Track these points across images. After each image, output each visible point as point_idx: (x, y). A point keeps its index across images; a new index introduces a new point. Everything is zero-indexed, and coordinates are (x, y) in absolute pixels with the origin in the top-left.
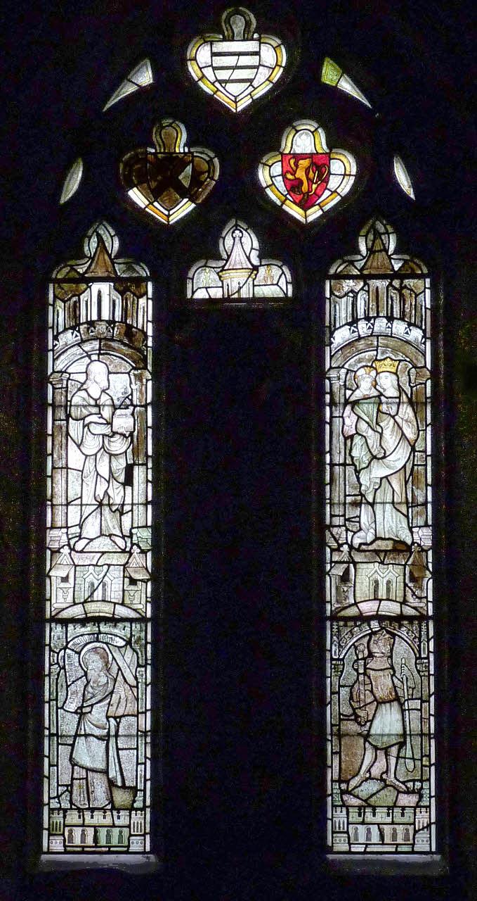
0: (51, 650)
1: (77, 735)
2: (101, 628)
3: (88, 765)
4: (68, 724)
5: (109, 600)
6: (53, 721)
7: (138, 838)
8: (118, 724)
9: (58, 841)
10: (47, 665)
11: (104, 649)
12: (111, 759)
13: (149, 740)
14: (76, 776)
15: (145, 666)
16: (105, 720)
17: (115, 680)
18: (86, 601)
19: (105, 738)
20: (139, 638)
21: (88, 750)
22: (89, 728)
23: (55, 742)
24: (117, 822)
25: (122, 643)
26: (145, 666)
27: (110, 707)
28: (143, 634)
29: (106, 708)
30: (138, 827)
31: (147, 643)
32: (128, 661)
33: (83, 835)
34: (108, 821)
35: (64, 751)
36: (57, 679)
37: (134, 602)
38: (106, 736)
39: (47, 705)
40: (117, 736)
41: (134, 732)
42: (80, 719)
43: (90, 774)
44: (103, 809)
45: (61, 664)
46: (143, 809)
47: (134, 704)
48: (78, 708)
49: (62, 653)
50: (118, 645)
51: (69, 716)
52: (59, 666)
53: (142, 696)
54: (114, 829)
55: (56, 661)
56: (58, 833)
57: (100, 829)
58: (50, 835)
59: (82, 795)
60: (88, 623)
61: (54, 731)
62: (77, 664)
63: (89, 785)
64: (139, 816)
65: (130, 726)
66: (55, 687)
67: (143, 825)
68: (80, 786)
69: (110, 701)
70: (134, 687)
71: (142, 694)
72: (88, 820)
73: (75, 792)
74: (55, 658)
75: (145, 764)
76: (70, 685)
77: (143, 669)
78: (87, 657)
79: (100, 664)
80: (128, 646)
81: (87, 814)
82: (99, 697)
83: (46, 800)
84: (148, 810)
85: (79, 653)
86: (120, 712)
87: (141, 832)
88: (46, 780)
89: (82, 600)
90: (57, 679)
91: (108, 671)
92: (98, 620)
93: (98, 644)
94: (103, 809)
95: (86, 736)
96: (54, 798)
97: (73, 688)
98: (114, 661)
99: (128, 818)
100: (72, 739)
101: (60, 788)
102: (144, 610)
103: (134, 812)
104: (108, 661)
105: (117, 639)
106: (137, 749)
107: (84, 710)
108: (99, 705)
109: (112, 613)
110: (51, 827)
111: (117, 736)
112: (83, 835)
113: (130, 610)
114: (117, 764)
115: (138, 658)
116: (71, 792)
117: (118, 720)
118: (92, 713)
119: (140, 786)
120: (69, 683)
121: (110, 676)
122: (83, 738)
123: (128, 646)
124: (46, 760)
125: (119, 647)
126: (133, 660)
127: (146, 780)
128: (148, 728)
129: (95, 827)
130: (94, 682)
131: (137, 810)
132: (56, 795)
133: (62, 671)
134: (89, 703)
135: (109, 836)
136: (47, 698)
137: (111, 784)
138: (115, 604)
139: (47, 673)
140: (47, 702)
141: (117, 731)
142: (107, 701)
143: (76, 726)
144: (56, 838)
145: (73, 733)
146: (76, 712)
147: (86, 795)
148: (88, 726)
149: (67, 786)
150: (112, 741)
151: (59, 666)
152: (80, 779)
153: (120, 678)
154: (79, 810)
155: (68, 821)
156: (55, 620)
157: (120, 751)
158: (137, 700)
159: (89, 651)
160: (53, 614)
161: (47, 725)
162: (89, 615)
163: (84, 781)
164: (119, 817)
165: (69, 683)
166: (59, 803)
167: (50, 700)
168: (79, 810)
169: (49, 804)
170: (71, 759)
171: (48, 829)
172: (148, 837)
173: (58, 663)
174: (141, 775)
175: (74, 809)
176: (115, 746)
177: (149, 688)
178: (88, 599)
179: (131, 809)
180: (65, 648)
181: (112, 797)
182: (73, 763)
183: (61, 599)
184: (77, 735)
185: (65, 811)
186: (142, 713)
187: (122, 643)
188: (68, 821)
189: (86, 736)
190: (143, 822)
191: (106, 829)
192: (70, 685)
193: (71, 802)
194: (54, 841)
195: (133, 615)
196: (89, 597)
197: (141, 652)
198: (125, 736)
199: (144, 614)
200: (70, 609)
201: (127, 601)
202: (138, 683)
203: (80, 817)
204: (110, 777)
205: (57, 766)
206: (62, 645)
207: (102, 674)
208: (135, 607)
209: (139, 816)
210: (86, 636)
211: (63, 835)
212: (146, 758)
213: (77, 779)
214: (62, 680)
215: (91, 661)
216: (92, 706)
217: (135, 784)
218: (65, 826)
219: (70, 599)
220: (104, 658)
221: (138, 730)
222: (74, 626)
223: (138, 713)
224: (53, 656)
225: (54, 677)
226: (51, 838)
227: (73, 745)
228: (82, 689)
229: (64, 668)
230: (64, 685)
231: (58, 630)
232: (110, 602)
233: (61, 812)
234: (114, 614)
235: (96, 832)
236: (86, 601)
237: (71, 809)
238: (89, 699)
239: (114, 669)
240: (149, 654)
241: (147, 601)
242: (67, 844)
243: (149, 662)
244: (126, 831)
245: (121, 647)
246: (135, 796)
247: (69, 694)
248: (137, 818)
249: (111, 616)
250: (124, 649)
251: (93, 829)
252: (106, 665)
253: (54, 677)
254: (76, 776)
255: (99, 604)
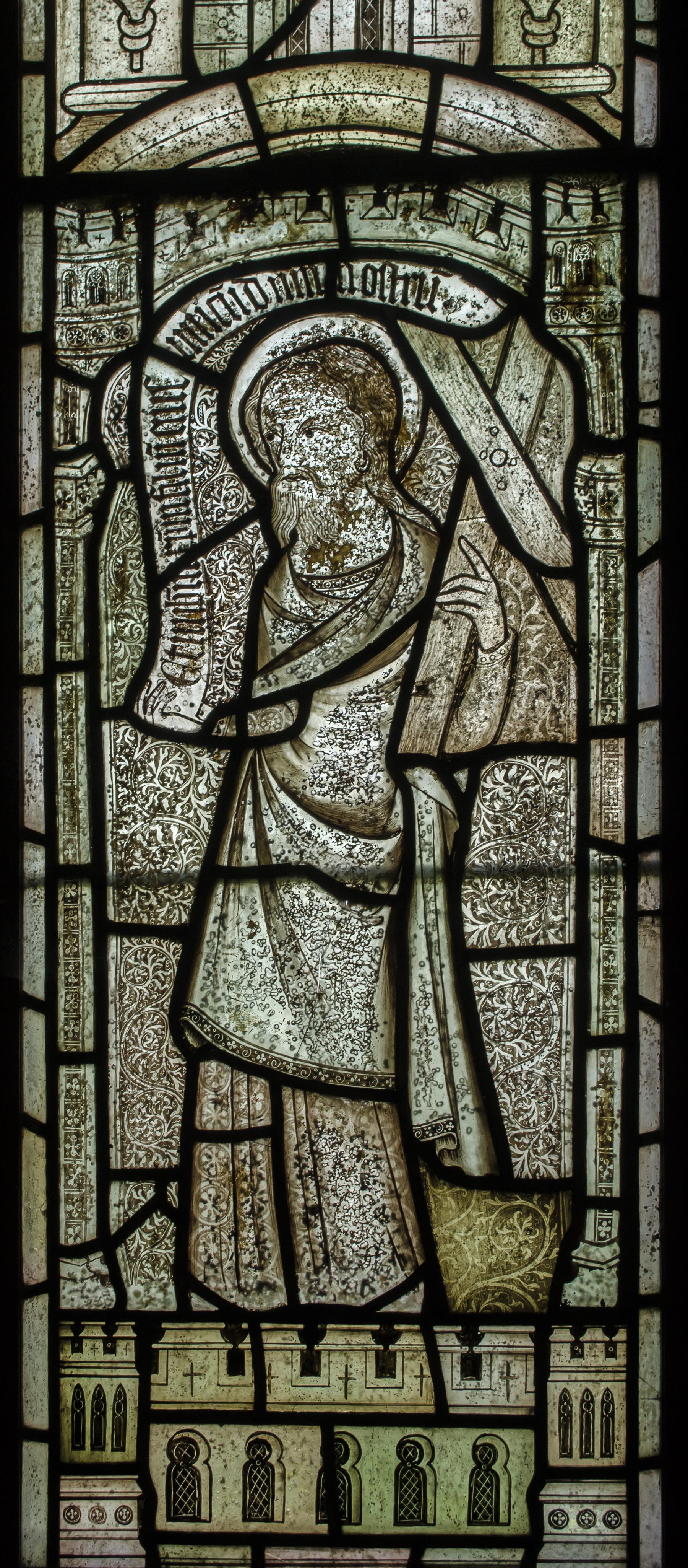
0: (52, 368)
1: (213, 875)
2: (353, 221)
3: (283, 1048)
4: (165, 809)
5: (401, 47)
6: (73, 803)
7: (591, 1490)
8: (464, 801)
9: (110, 1507)
10: (32, 460)
11: (376, 354)
12: (422, 1013)
13: (649, 894)
14: (210, 1116)
15: (626, 448)
16: (382, 781)
17: (444, 536)
18: (260, 62)
19: (387, 894)
20: (589, 274)
21: (280, 963)
22: (284, 830)
23: (86, 918)
24: (462, 1396)
25: (473, 306)
26: (626, 448)
27: (414, 702)
28: (609, 252)
29: (388, 708)
30: (587, 1421)
31: (633, 302)
32: (521, 415)
33: (259, 1473)
34: (409, 1389)
35: (139, 970)
36: (93, 542)
37: (560, 54)
38: (390, 877)
39: (650, 1278)
40: (455, 872)
41: (560, 848)
42: (230, 775)
43: (296, 1105)
44: (375, 1318)
45: (117, 447)
46: (619, 1317)
47: (563, 678)
48: (221, 711)
49: (118, 386)
50: (459, 317)
51: (166, 761)
52: (105, 462)
53: (610, 632)
54: (439, 1437)
55: (81, 434)
56: (110, 1456)
57: (359, 1432)
58: (59, 1468)
59: (248, 1234)
60: (275, 195)
61: (76, 849)
62: (208, 449)
63: (293, 1173)
64: (595, 1357)
65: (535, 811)
66: (80, 591)
67: (620, 1414)
68: (235, 1178)
69: (411, 667)
70: (557, 573)
71: (610, 613)
72: (286, 1384)
73: (205, 1214)
74: (81, 417)
75: (629, 1040)
76: (173, 572)
77: (612, 466)
78: (270, 400)
79: (348, 442)
80: (521, 325)
81: (282, 1347)
82: (344, 644)
83: (35, 1267)
84: (650, 1323)
85: (221, 382)
86: (477, 725)
87: (608, 1452)
88: (33, 1146)
89: (237, 57)
90: (93, 542)
91: (397, 480)
92: (331, 172)
93: (336, 325)
94: (375, 1318)
95: (271, 874)
96: (82, 1251)
97: (189, 590)
98: (433, 425)
99: (523, 1373)
100: (186, 896)
101: (116, 1192)
102: (615, 101)
103: (562, 1334)
104: (399, 420)
105: (454, 285)
106: (579, 950)
107: (259, 724)
108: (343, 691)
109: (419, 124)
110: (67, 1420)
111: (455, 872)
112: (259, 1473)
113: (526, 111)
114: (458, 1046)
115: (581, 395)
116: (183, 1220)
117: (462, 777)
118: (308, 738)
119: (602, 1176)
120: (163, 563)
121: (413, 514)
122: (251, 891)
123: (521, 325)
124: (34, 1025)
125: (460, 334)
126: (551, 411)
127: (633, 1141)
128: (648, 823)
129: (325, 1421)
130: (313, 554)
131: (581, 1319)
132: (90, 1231)
133: (123, 492)
134: (286, 678)
135: (411, 1477)
136: (32, 658)
137: (424, 1161)
138: (438, 70)
139: (31, 502)
140: (33, 681)
141: (458, 845)
142: (396, 667)
143: (206, 816)
144: (98, 1486)
145: (187, 860)
146: (204, 738)
147: (270, 1233)
148: (281, 814)
149: (159, 1177)
150: (429, 900)
151: (105, 462)
152: (234, 1137)
153: (471, 525)
154: (238, 1323)
155: (169, 1389)
156: (72, 185)
157: (479, 972)
158: (579, 648)
159: (279, 363)
160: (65, 148)
161: (34, 814)
162: (278, 146)
163: (262, 1147)
164: (471, 1367)
165: (163, 563)
166: (114, 1278)
167: (54, 667)
168: (238, 1323)
169: (51, 1286)
170: (179, 1014)
171: (50, 1437)
172: (650, 1484)
173: (95, 445)
174: (604, 1112)
175: (204, 1317)
176: (442, 932)
177: (649, 582)
178: (271, 45)
179: (547, 1315)
180: (141, 351)
181: (429, 1243)
182: (197, 1045)
183: (110, 61)
184: (213, 875)
185: (149, 1326)
186: (608, 731)
187: (473, 306)
188: (169, 1389)
189: (271, 874)
190: (619, 1392)
191: (395, 1435)
192: (173, 572)
193: (183, 1276)
194: (85, 1507)
195: (546, 132)
196: (279, 35)
197: (602, 355)
198: (502, 873)
199: (614, 128)
200: (164, 116)
201: (511, 50)
202: (581, 548)
203: (235, 1366)
204: (418, 1120)
205: (98, 1057)
206: (121, 332)
207: (362, 500)
208: (560, 83)
209: (595, 1357)
210: (262, 278)
211: (139, 1469)
212: (634, 1003)
213: (217, 1137)
214: (120, 540)
215: (292, 428)
216: (303, 695)
217: (567, 1162)
218: (149, 1416)
219: (162, 55)
220: (374, 401)
221: (585, 841)
222: (191, 219)
223: (588, 732)
224: (70, 403)
225: (73, 527)
226: (69, 1486)
227: (189, 936)
228: (242, 595)
229: (133, 472)
230: (136, 574)
231: (95, 249)
232: (409, 61)
233: (126, 1331)
234: (429, 133)
235: (333, 1455)
236: (260, 62)
237: (184, 1314)
238: (287, 656)
239: (438, 467)
240: (649, 375)
241: (632, 49)
242: (161, 1522)
243: (650, 418)
244: (516, 1444)
245: (481, 333)
246: (572, 1236)
247: (167, 627)
248: (584, 1371)
249: (413, 144)
250: (494, 345)
251: (313, 1435)
252: (389, 447)
253: (73, 527)
254: (210, 1116)
255: (339, 77)
